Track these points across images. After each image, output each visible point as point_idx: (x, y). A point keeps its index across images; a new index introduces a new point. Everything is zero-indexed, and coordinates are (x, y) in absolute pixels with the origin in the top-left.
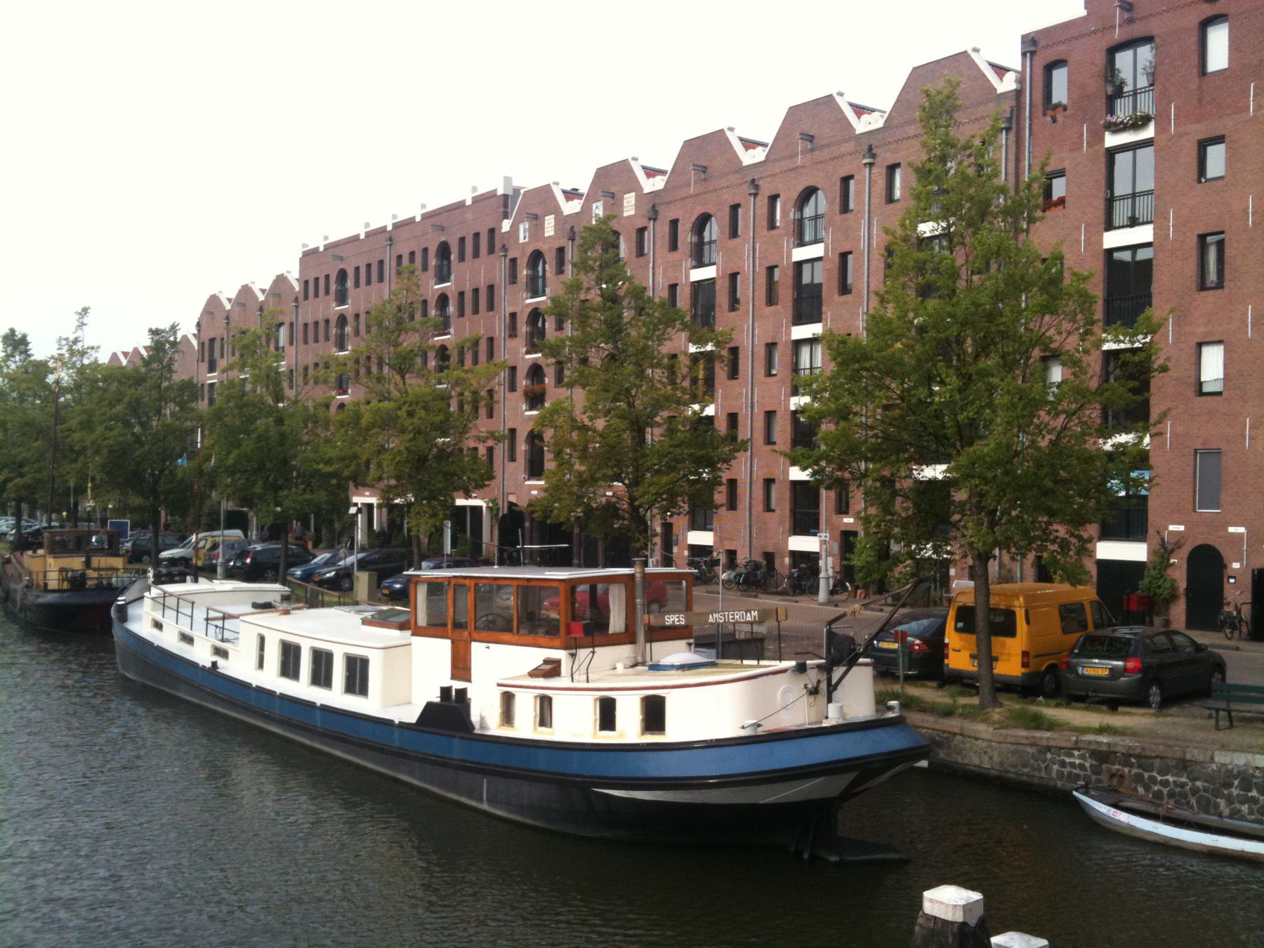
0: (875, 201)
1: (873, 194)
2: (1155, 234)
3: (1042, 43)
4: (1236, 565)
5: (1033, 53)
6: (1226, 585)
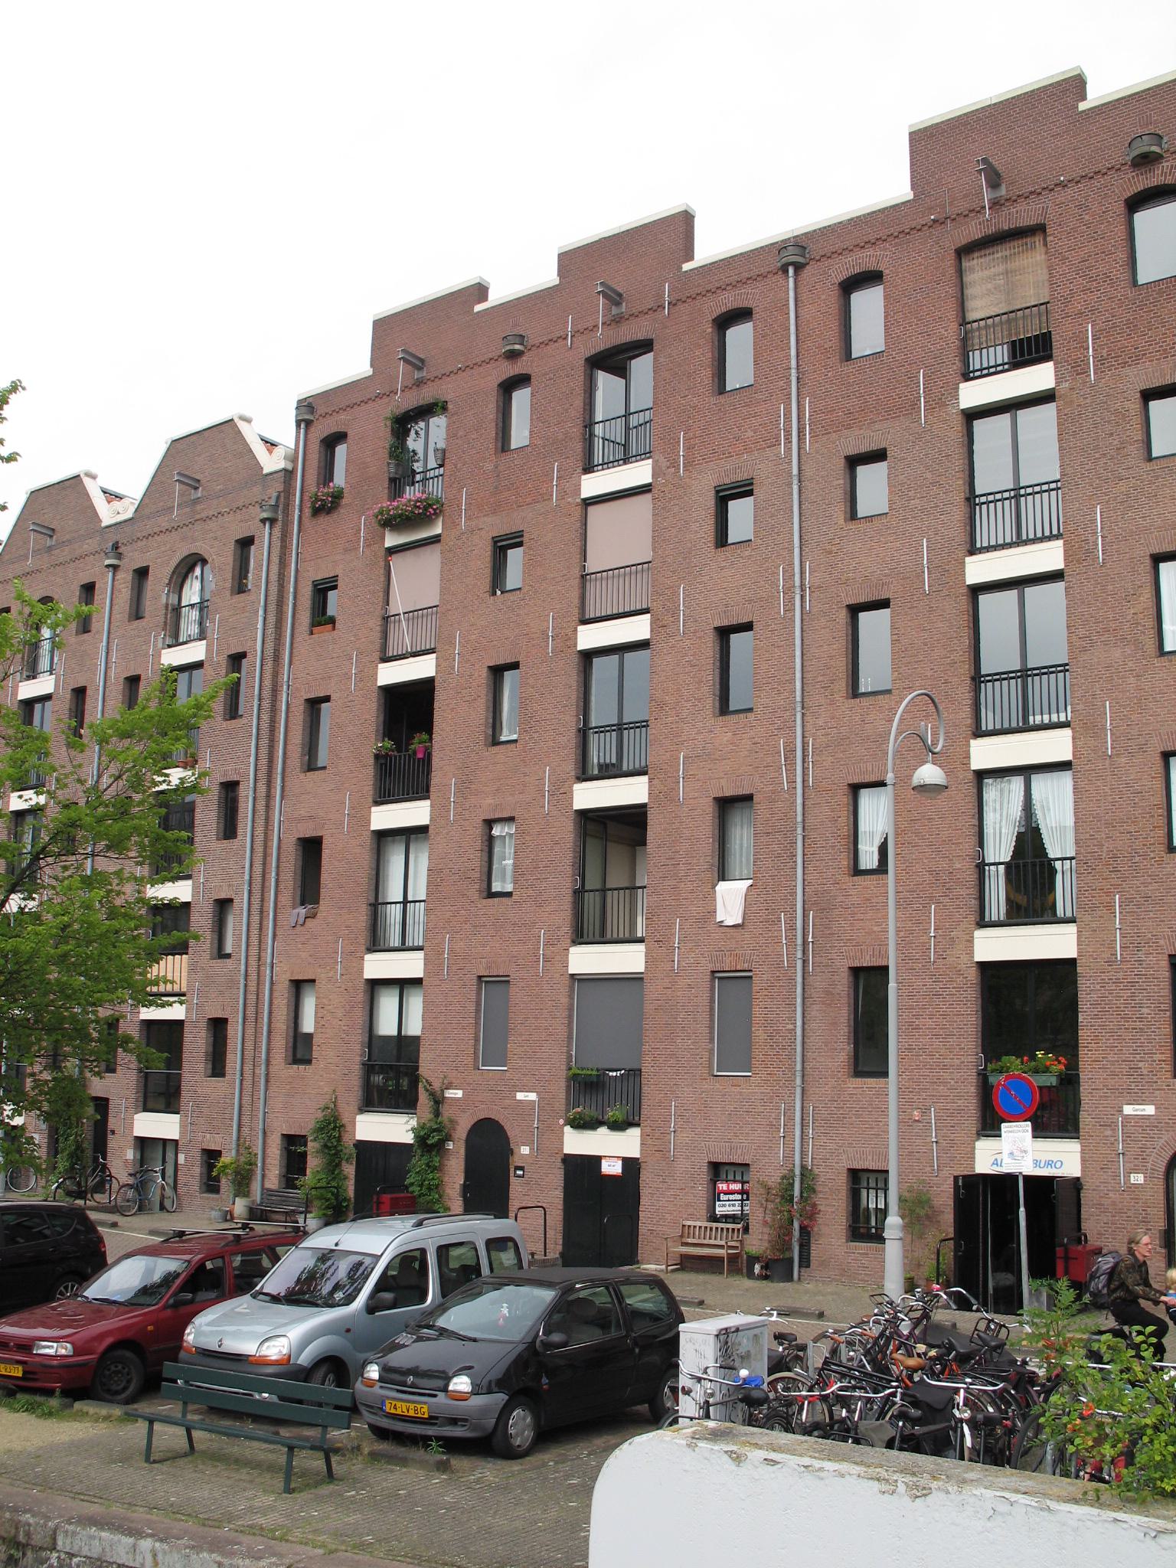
0: (116, 616)
1: (116, 607)
2: (438, 666)
3: (321, 410)
4: (525, 1150)
5: (309, 423)
6: (512, 1179)
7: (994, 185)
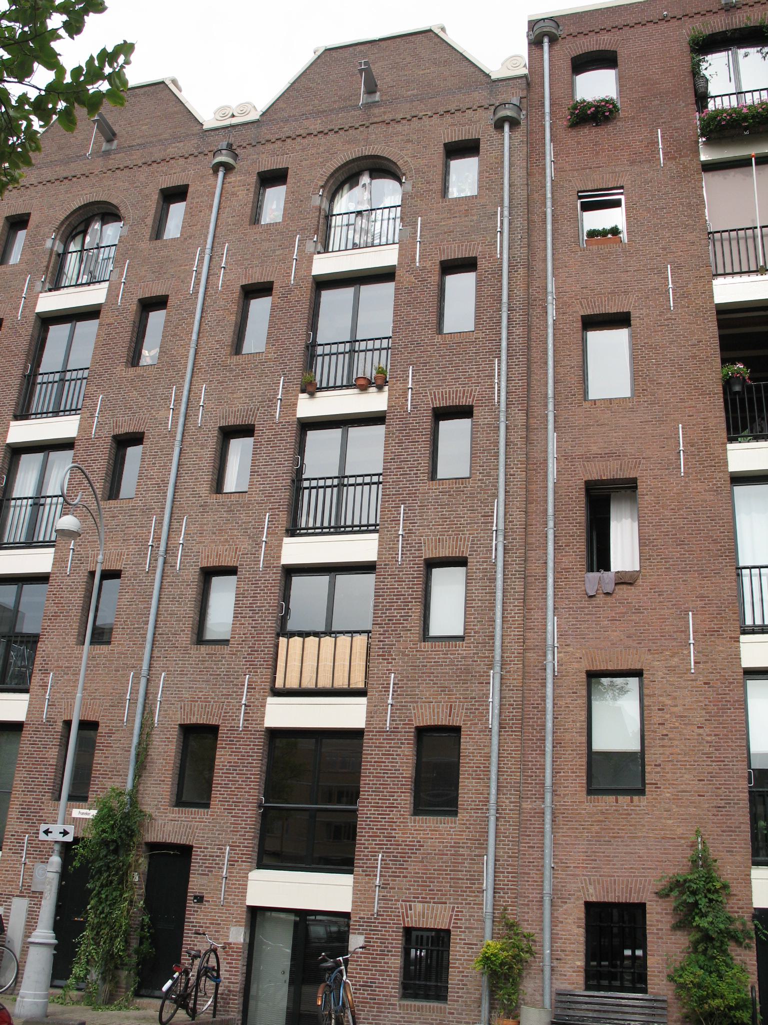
7: (371, 90)
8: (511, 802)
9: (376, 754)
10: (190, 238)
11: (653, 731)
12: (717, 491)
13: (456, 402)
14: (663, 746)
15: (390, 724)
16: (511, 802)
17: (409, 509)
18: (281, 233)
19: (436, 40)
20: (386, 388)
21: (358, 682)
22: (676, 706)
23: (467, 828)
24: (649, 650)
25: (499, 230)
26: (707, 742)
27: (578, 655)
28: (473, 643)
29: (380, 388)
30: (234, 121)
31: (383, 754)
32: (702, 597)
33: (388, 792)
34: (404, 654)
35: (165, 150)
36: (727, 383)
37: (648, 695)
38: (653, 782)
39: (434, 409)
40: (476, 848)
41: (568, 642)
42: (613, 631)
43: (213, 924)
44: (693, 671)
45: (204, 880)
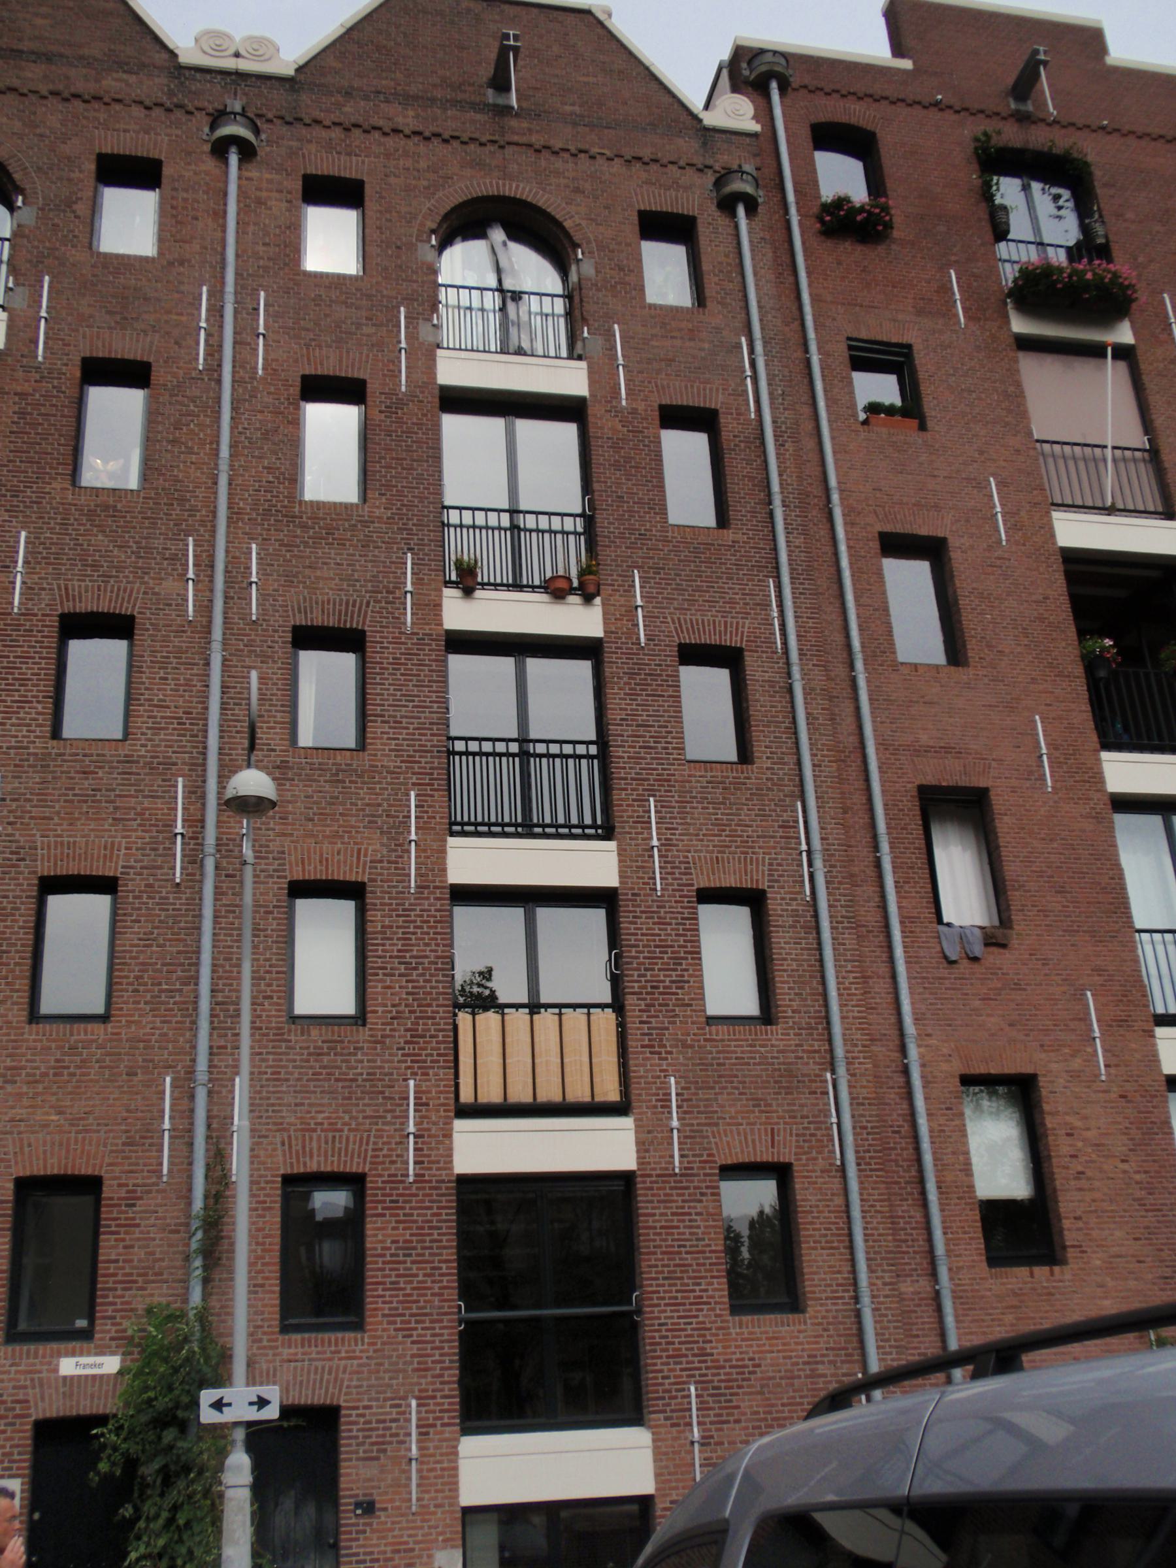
8: (885, 1284)
9: (662, 1214)
10: (182, 263)
11: (1064, 1167)
12: (1098, 818)
13: (714, 640)
14: (1080, 1189)
15: (680, 1162)
16: (885, 1284)
17: (662, 805)
18: (369, 297)
19: (599, 30)
20: (598, 600)
21: (610, 1092)
22: (1088, 1129)
23: (825, 1330)
24: (1042, 1046)
25: (749, 373)
26: (1137, 1183)
27: (945, 1051)
28: (792, 1028)
29: (588, 599)
30: (244, 65)
31: (673, 1214)
32: (1098, 970)
33: (689, 1278)
34: (685, 1045)
35: (97, 81)
36: (1091, 664)
37: (1049, 1113)
38: (1076, 1243)
39: (680, 645)
40: (843, 1362)
41: (930, 1031)
42: (989, 1015)
43: (399, 1551)
44: (1103, 1078)
45: (369, 1471)
